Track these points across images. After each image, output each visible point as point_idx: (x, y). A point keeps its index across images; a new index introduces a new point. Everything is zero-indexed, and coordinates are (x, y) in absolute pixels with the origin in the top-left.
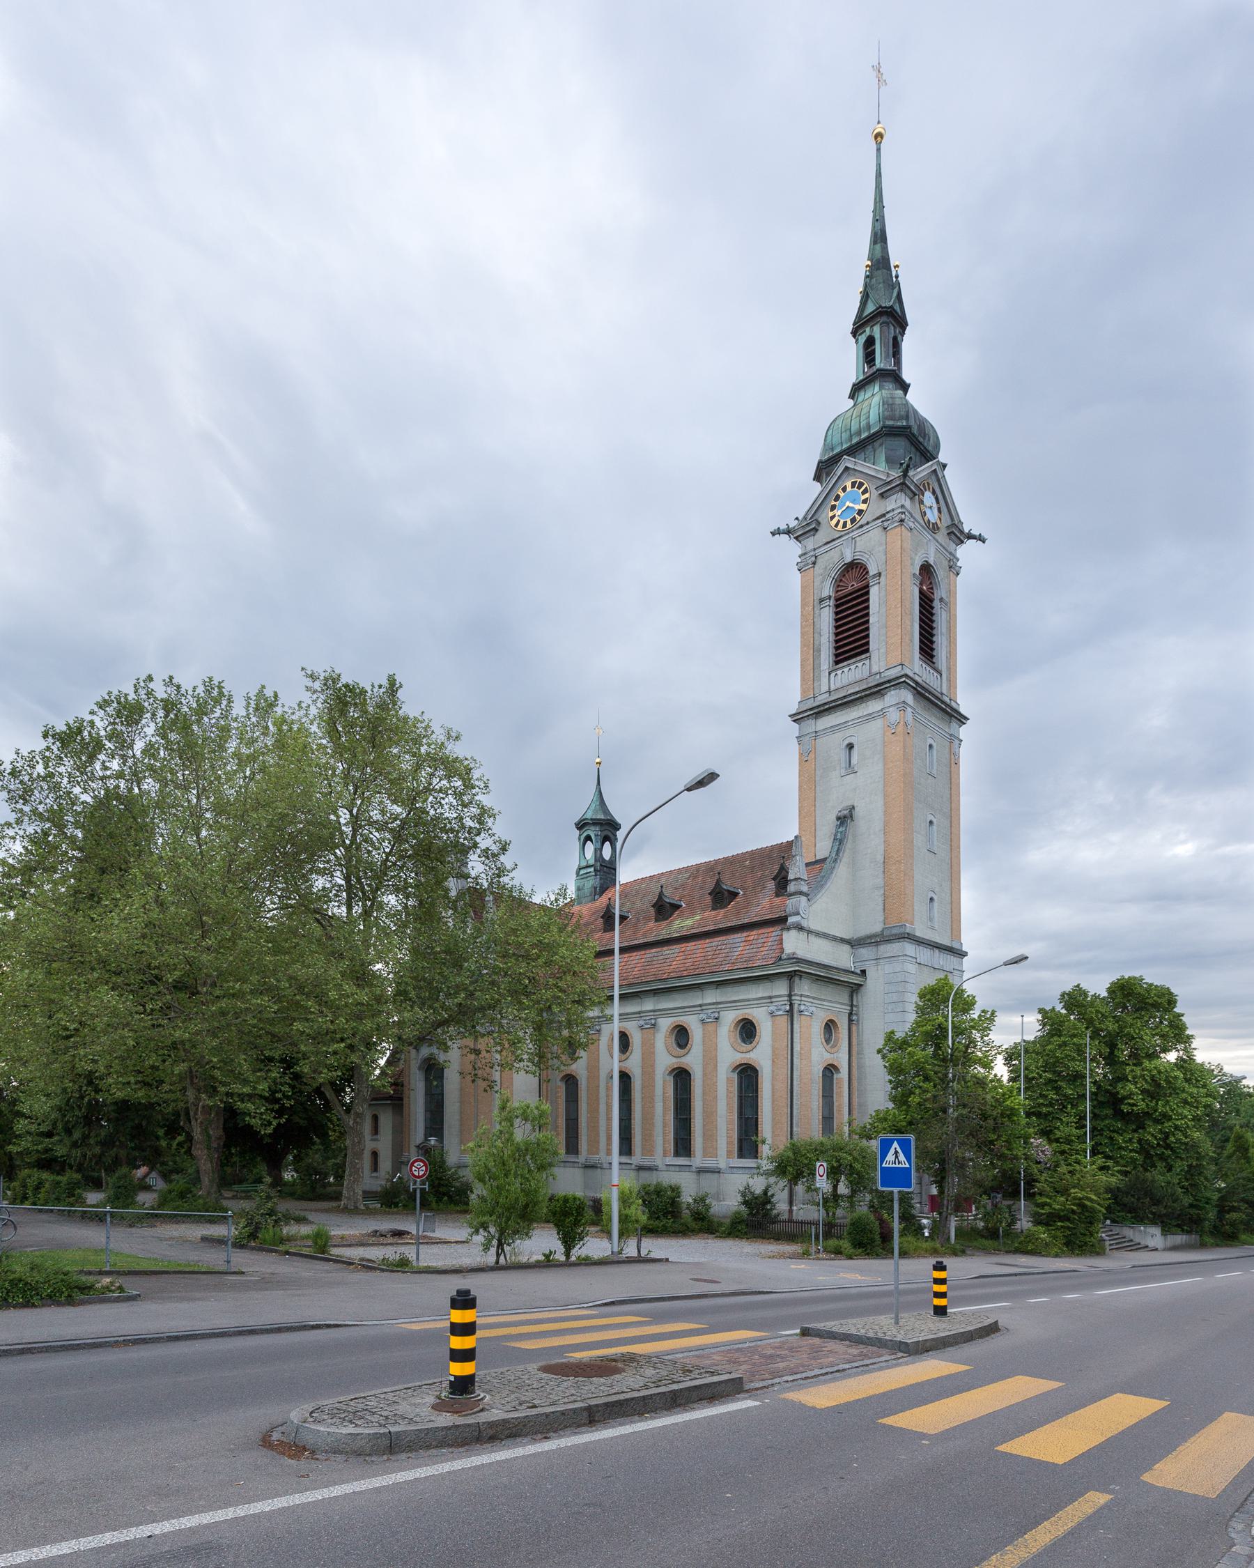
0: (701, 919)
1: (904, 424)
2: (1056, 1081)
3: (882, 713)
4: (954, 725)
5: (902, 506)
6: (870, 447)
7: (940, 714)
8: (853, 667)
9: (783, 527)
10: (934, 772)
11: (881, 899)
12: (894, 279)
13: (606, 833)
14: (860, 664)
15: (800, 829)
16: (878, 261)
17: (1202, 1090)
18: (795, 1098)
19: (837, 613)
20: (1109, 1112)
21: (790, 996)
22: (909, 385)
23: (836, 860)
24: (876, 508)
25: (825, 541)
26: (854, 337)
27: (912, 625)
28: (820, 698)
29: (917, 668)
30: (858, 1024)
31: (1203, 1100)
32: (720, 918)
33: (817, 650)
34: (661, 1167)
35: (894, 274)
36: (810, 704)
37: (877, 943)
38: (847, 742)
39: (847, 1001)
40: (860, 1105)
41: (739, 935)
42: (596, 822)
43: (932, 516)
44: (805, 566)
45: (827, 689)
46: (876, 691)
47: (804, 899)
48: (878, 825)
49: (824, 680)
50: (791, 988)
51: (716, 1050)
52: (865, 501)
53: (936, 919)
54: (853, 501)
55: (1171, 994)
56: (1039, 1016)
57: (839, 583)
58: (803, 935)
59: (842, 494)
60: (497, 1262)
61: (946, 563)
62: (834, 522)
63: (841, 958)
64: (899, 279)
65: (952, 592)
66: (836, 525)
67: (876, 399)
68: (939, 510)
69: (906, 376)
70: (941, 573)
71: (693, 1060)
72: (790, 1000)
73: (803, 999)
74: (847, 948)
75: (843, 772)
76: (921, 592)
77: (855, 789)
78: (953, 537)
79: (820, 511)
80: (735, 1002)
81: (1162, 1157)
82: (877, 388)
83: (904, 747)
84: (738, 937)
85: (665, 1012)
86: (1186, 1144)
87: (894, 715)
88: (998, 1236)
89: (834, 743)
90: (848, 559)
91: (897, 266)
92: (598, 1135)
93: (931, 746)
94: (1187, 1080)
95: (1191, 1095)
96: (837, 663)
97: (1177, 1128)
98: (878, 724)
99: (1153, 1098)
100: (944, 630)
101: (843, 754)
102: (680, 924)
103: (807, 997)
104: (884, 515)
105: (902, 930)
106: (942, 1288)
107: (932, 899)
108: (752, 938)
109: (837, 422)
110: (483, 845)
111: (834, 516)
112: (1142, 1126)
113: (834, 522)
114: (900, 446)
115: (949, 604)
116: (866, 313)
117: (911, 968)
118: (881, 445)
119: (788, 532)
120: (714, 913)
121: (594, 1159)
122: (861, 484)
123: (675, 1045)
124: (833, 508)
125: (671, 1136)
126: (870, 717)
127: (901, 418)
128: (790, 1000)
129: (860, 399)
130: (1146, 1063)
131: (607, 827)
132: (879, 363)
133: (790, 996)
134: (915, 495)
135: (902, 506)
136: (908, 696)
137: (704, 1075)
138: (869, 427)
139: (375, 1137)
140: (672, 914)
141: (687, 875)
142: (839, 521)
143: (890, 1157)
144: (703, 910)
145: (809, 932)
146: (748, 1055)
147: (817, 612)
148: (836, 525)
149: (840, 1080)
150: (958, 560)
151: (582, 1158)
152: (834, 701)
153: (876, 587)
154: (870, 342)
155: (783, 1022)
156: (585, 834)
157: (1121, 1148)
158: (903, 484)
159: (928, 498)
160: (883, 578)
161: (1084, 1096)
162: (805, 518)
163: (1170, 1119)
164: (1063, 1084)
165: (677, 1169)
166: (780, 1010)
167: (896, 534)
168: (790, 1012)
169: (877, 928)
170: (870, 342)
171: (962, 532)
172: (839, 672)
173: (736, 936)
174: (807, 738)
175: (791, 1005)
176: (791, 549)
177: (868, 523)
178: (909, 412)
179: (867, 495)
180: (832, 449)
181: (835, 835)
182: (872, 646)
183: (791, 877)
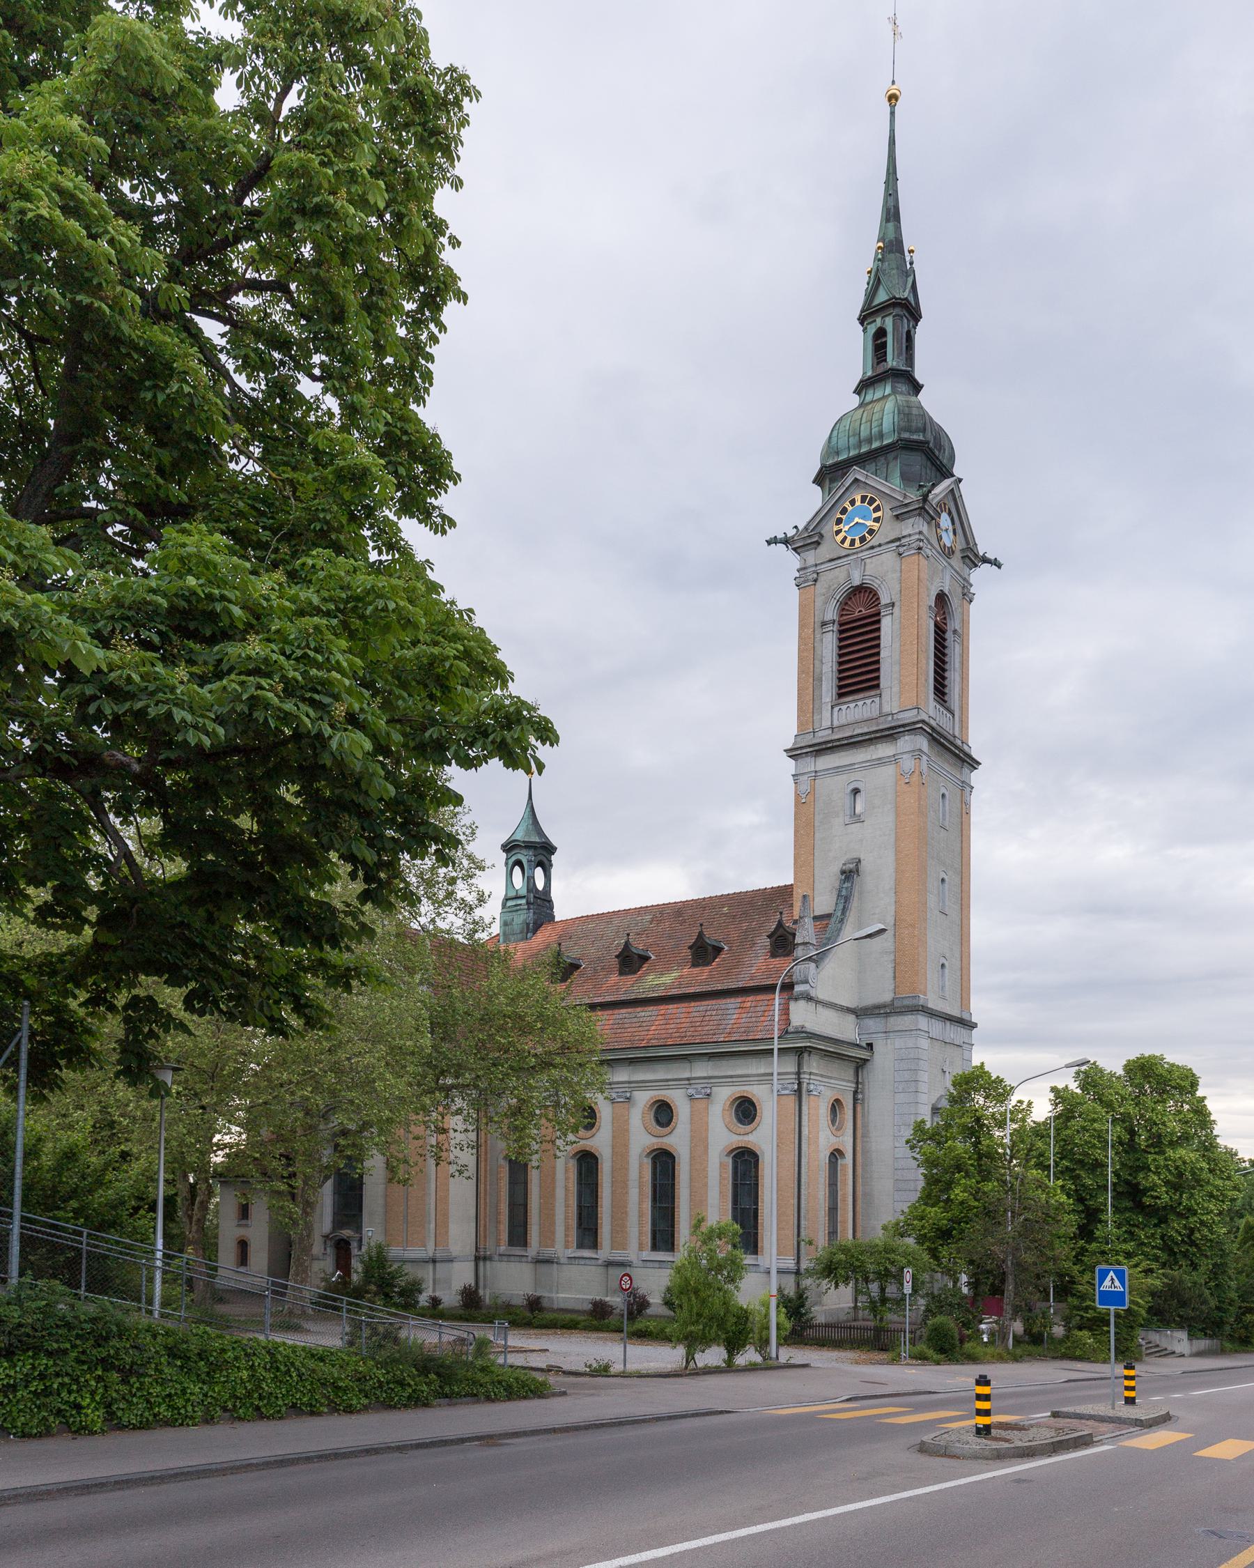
0: (681, 977)
1: (921, 438)
2: (1074, 1170)
3: (894, 759)
4: (966, 770)
5: (920, 533)
6: (882, 459)
7: (952, 760)
8: (860, 703)
10: (947, 823)
11: (891, 965)
13: (540, 858)
14: (868, 701)
15: (795, 879)
16: (891, 242)
17: (1227, 1183)
18: (803, 1187)
19: (841, 640)
20: (1129, 1204)
21: (798, 1073)
22: (922, 387)
23: (842, 921)
24: (888, 530)
25: (829, 557)
26: (862, 323)
27: (928, 663)
28: (820, 734)
29: (931, 710)
30: (863, 1104)
31: (1230, 1193)
32: (702, 977)
33: (818, 680)
34: (635, 1262)
35: (908, 259)
36: (809, 740)
37: (887, 1015)
38: (852, 786)
39: (852, 1078)
40: (865, 1194)
41: (732, 1000)
42: (529, 846)
43: (948, 540)
44: (805, 582)
46: (890, 734)
47: (813, 965)
48: (888, 882)
49: (826, 714)
50: (800, 1065)
51: (707, 1130)
52: (877, 520)
53: (947, 988)
54: (864, 518)
55: (1194, 1075)
56: (1052, 1096)
57: (844, 606)
58: (811, 1006)
59: (850, 508)
60: (686, 1368)
61: (960, 590)
62: (839, 538)
63: (844, 1029)
65: (965, 622)
66: (843, 541)
67: (890, 405)
68: (955, 533)
69: (919, 375)
70: (955, 601)
71: (678, 1140)
72: (799, 1079)
74: (852, 1018)
75: (847, 820)
76: (936, 625)
77: (861, 840)
78: (967, 560)
79: (824, 522)
80: (731, 1077)
81: (1185, 1255)
82: (888, 390)
83: (920, 799)
84: (731, 1003)
85: (643, 1085)
86: (1211, 1241)
87: (908, 763)
88: (1042, 1341)
89: (835, 788)
90: (857, 582)
91: (911, 251)
92: (553, 1223)
93: (943, 795)
94: (1211, 1171)
95: (1217, 1188)
96: (840, 695)
97: (1202, 1223)
98: (889, 770)
99: (1176, 1190)
100: (957, 665)
101: (848, 800)
102: (655, 981)
103: (816, 1074)
104: (899, 539)
105: (915, 1002)
106: (1132, 1383)
107: (943, 966)
108: (749, 1004)
109: (843, 423)
110: (460, 895)
111: (840, 531)
112: (1163, 1220)
113: (839, 538)
114: (916, 461)
115: (962, 636)
116: (876, 302)
117: (924, 1043)
118: (895, 458)
119: (786, 541)
120: (696, 970)
121: (548, 1252)
122: (872, 501)
123: (654, 1123)
124: (839, 521)
125: (648, 1228)
126: (881, 762)
127: (917, 431)
128: (799, 1079)
129: (869, 398)
130: (1170, 1153)
131: (541, 851)
132: (892, 361)
133: (798, 1073)
134: (933, 518)
135: (920, 533)
136: (923, 743)
137: (692, 1158)
138: (881, 436)
139: (243, 1222)
140: (640, 967)
141: (648, 917)
142: (845, 538)
143: (1107, 1282)
144: (680, 966)
145: (818, 1002)
146: (746, 1138)
147: (818, 636)
148: (843, 541)
149: (844, 1166)
151: (532, 1251)
152: (839, 740)
153: (889, 618)
154: (881, 333)
155: (791, 1102)
156: (514, 859)
157: (1143, 1244)
158: (923, 508)
159: (945, 520)
160: (896, 610)
161: (1106, 1187)
162: (806, 528)
163: (1195, 1213)
164: (1082, 1173)
165: (657, 1265)
166: (785, 1089)
167: (913, 561)
168: (799, 1092)
169: (887, 997)
170: (881, 333)
171: (976, 555)
172: (844, 707)
173: (728, 1001)
174: (805, 777)
175: (800, 1084)
176: (790, 561)
177: (880, 545)
178: (926, 423)
179: (879, 514)
180: (838, 453)
181: (840, 891)
182: (884, 682)
183: (798, 940)
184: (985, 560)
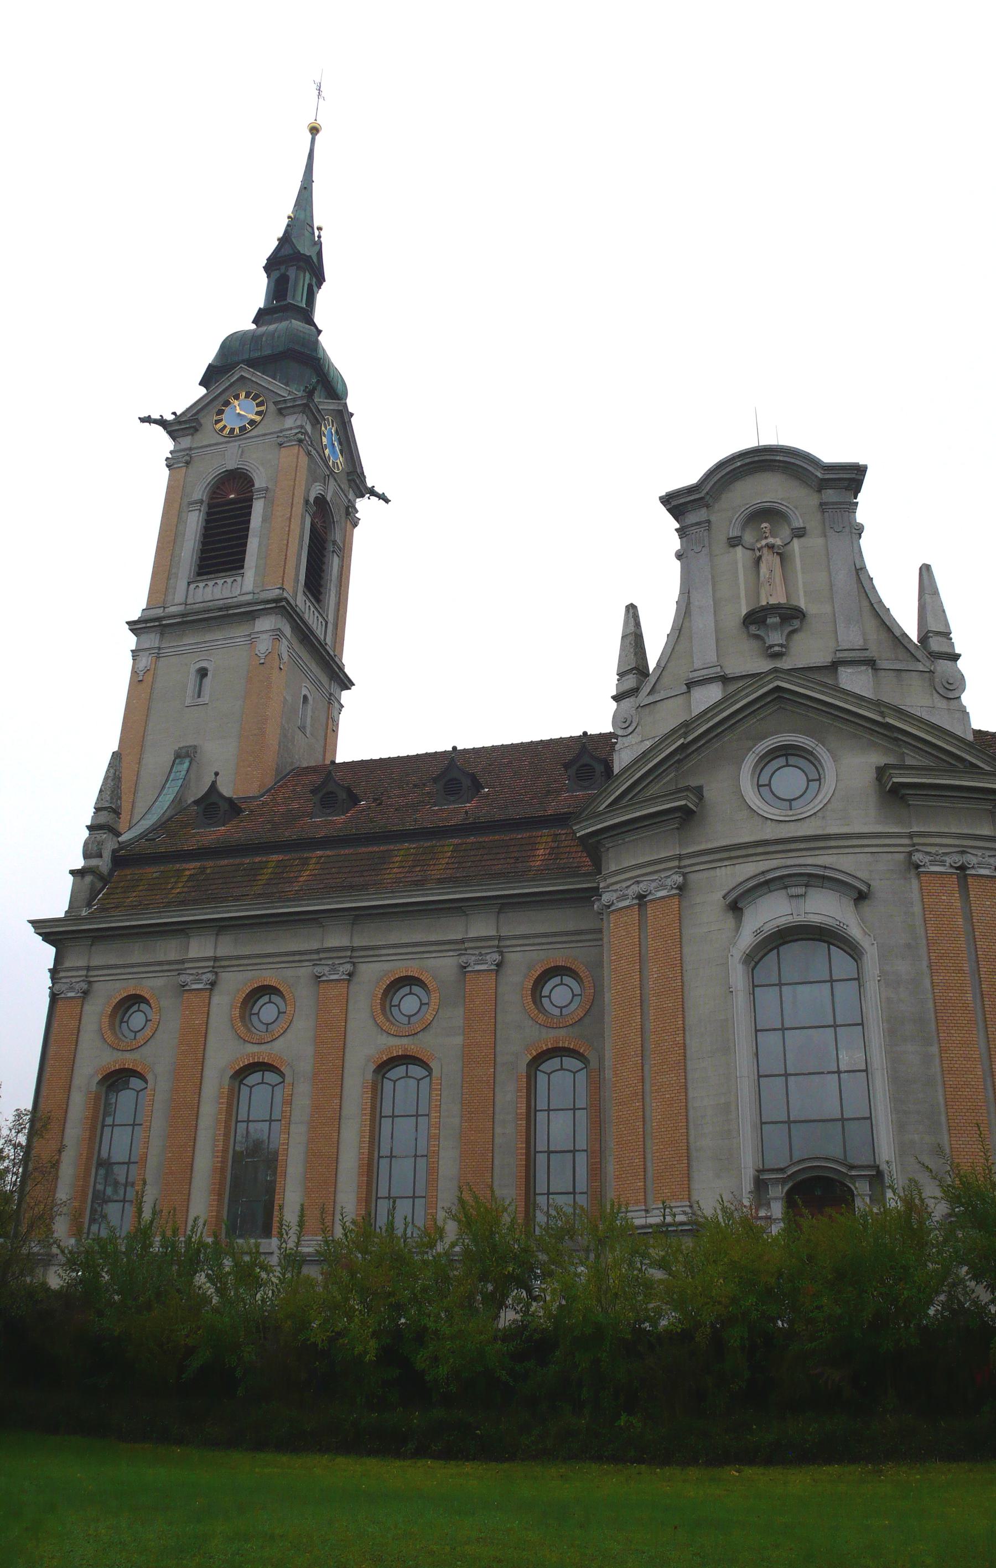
3: (460, 946)
4: (334, 688)
5: (302, 427)
9: (156, 416)
12: (316, 239)
38: (198, 666)
45: (182, 600)
49: (182, 584)
64: (322, 239)
73: (916, 840)
78: (353, 484)
90: (231, 466)
91: (320, 229)
96: (199, 574)
119: (162, 422)
142: (225, 427)
150: (357, 511)
166: (624, 897)
172: (201, 585)
184: (372, 492)
